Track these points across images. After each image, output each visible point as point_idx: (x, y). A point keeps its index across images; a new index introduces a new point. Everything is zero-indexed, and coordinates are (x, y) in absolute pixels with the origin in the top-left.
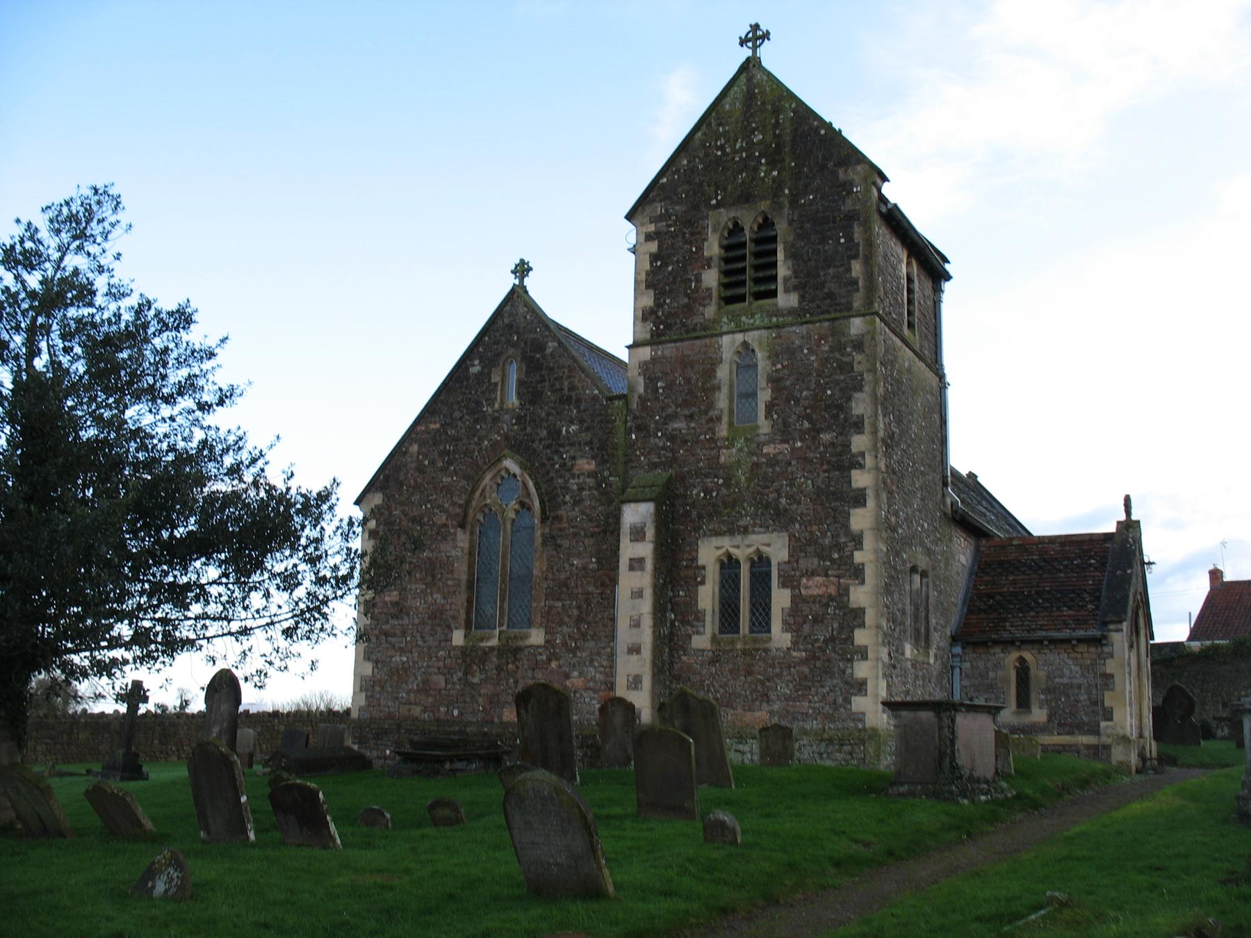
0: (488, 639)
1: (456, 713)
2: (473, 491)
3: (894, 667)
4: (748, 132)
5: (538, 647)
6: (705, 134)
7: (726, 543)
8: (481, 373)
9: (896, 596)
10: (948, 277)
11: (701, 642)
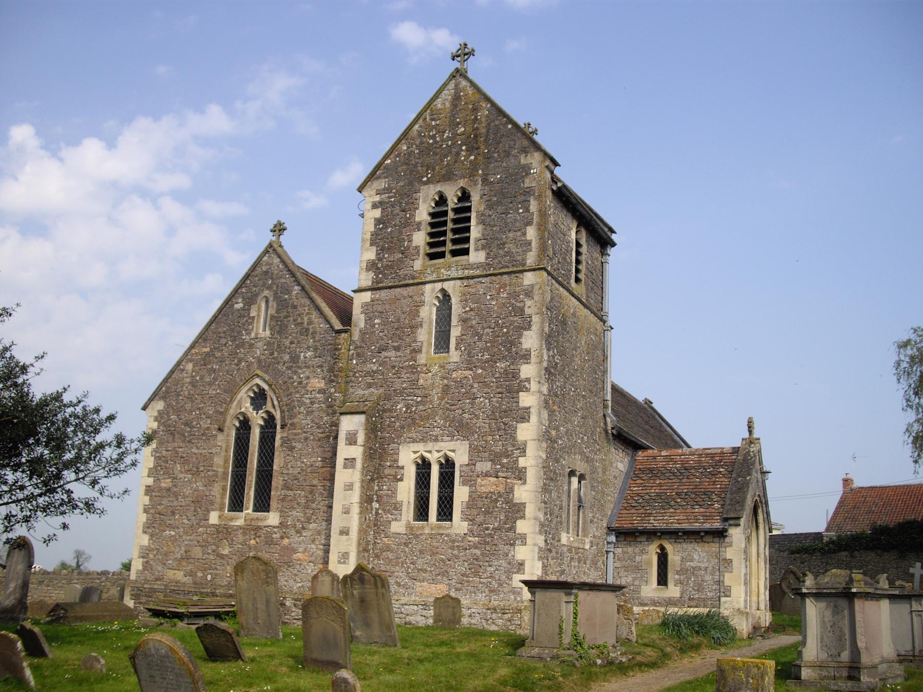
0: (237, 518)
1: (209, 577)
2: (231, 401)
3: (550, 551)
4: (454, 125)
5: (274, 527)
6: (421, 126)
7: (421, 448)
8: (243, 309)
9: (554, 495)
10: (613, 244)
11: (398, 527)
